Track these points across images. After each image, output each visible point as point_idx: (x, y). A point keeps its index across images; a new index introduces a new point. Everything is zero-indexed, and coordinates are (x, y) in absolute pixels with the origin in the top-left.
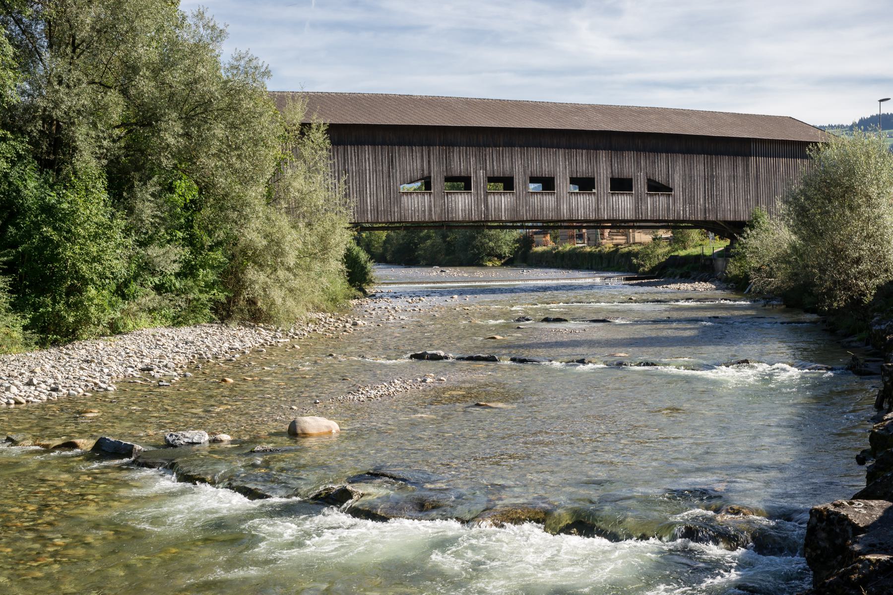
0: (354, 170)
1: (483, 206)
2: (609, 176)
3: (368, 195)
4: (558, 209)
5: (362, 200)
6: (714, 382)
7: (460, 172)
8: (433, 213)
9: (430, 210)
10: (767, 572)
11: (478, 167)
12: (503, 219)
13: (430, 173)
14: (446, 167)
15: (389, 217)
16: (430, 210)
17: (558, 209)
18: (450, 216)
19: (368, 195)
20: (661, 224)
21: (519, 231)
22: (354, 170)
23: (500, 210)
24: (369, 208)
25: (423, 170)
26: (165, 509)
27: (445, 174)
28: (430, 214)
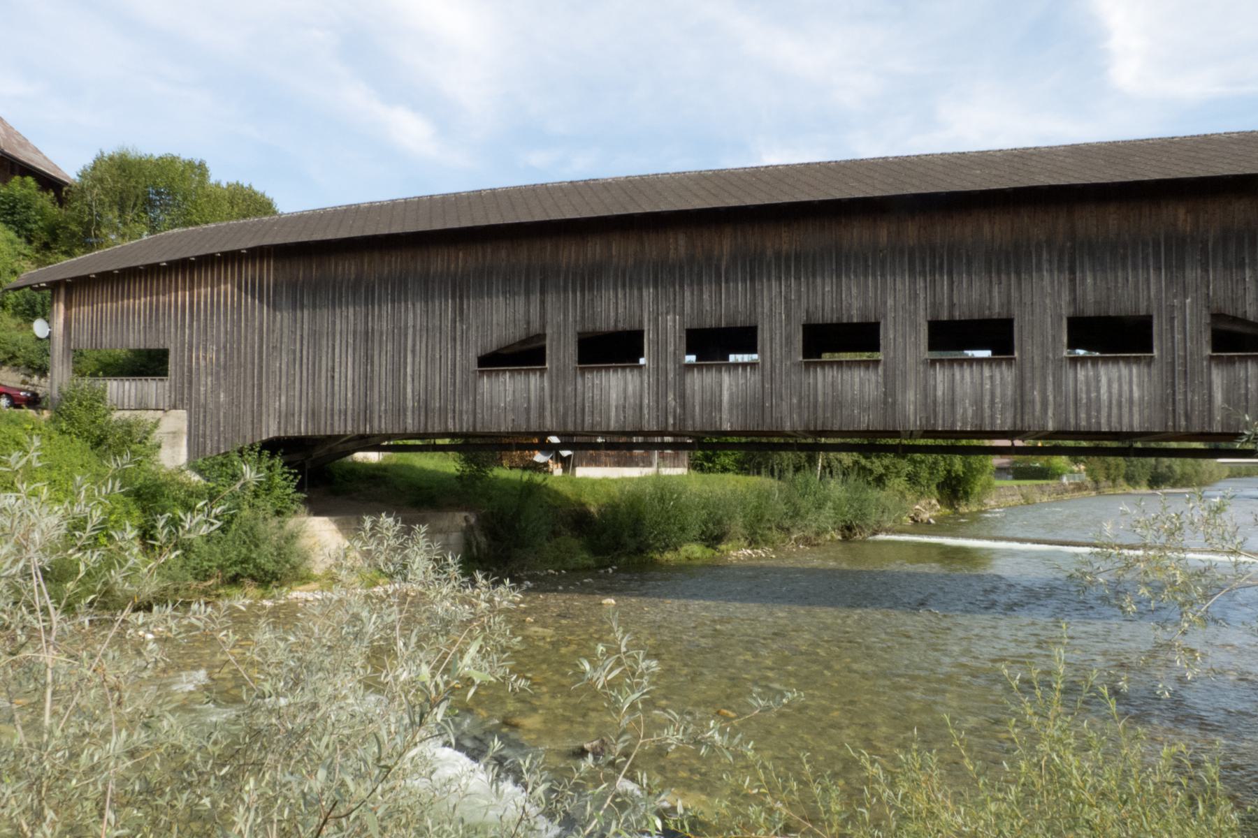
0: (384, 328)
1: (671, 397)
2: (1066, 311)
3: (409, 379)
4: (889, 399)
5: (396, 388)
6: (731, 395)
7: (616, 321)
8: (547, 414)
9: (542, 408)
10: (963, 666)
11: (662, 308)
12: (727, 427)
13: (543, 326)
14: (583, 312)
15: (450, 422)
16: (542, 408)
17: (889, 399)
18: (588, 419)
19: (409, 379)
20: (838, 440)
21: (1012, 291)
22: (384, 328)
23: (715, 404)
24: (410, 404)
25: (528, 323)
26: (1045, 273)
27: (578, 329)
28: (541, 415)
